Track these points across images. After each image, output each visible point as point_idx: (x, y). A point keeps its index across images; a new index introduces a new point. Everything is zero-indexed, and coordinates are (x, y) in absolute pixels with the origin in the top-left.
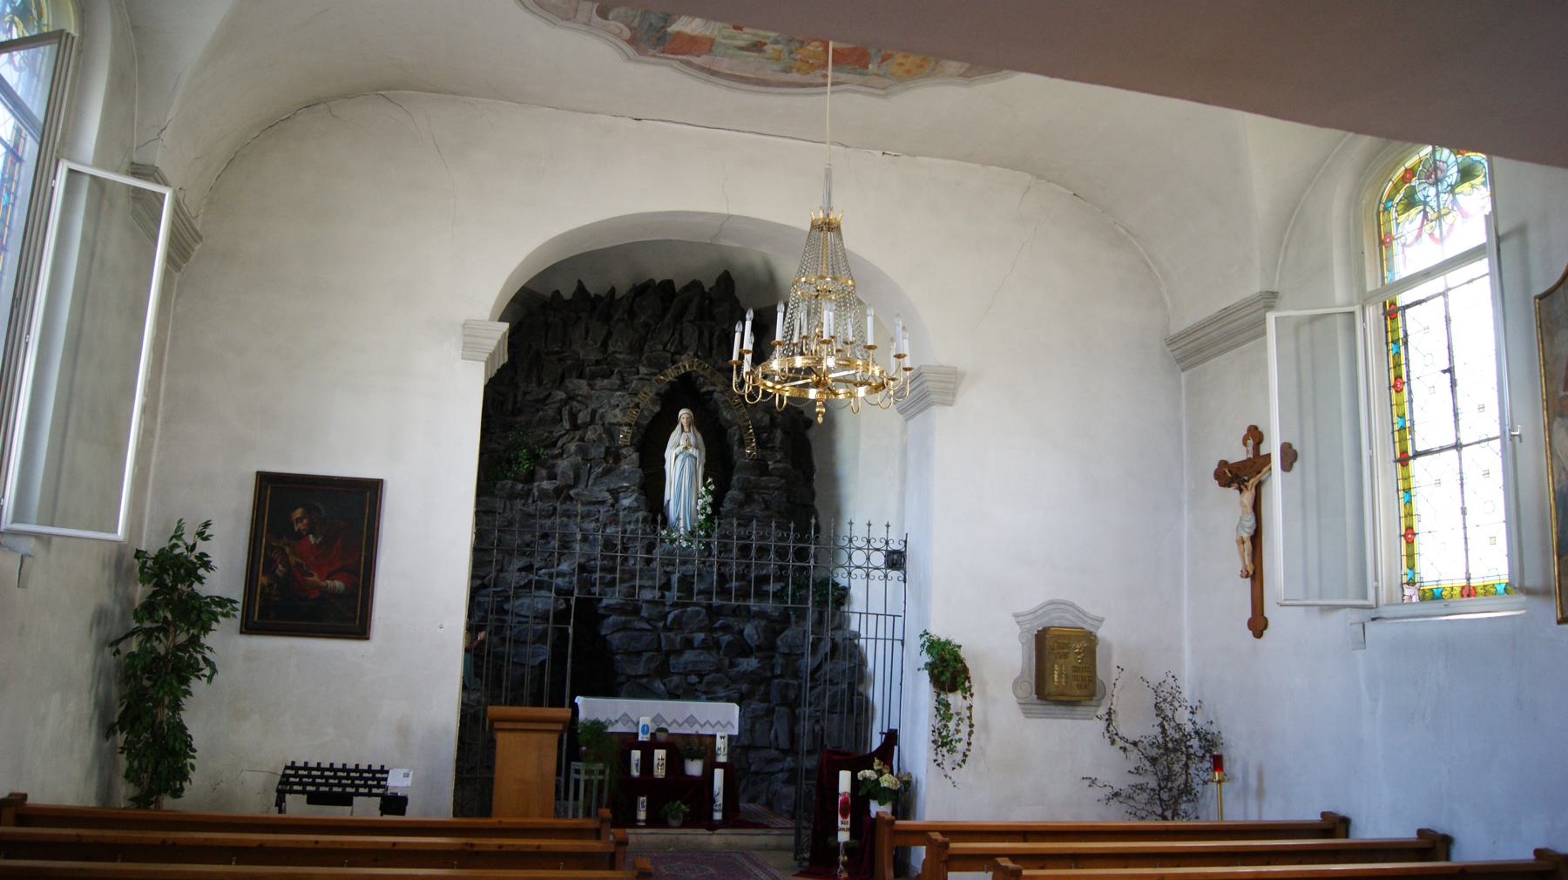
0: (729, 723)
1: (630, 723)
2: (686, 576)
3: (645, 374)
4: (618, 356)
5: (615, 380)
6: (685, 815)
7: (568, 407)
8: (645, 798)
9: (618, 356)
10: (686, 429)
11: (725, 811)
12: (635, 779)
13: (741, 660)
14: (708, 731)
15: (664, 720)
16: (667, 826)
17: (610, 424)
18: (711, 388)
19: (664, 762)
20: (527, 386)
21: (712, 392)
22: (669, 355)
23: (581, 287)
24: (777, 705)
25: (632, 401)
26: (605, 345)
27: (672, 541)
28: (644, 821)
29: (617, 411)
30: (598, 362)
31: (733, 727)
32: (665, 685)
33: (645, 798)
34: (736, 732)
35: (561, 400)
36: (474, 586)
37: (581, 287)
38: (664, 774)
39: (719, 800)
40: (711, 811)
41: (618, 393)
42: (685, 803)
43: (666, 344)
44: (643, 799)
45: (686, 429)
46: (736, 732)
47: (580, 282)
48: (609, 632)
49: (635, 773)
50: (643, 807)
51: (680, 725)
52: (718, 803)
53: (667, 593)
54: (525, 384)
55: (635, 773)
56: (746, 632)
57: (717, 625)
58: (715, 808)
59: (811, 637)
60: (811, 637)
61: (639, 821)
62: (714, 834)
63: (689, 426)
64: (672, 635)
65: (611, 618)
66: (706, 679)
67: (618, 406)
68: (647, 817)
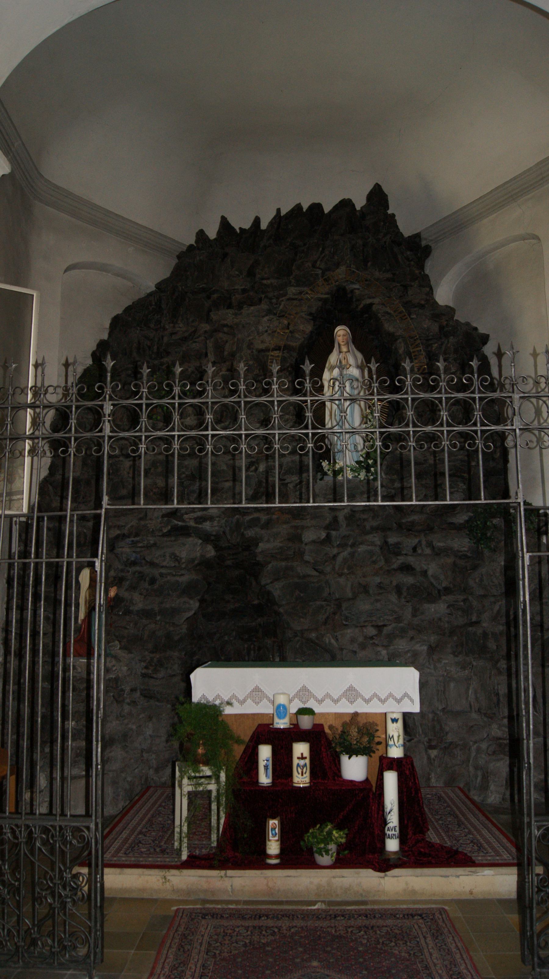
0: (406, 695)
1: (265, 700)
2: (354, 511)
3: (294, 295)
4: (265, 282)
5: (264, 306)
6: (341, 848)
7: (212, 340)
8: (276, 822)
9: (265, 282)
10: (344, 349)
11: (403, 839)
12: (265, 790)
13: (426, 606)
14: (375, 708)
15: (311, 695)
16: (313, 865)
17: (260, 351)
18: (368, 301)
19: (307, 761)
20: (174, 327)
21: (371, 304)
22: (320, 272)
23: (225, 224)
24: (268, 882)
25: (280, 323)
26: (251, 274)
27: (336, 473)
28: (277, 857)
29: (265, 337)
30: (244, 291)
31: (412, 701)
32: (337, 640)
33: (276, 822)
34: (416, 708)
35: (206, 332)
36: (111, 536)
37: (225, 224)
38: (307, 780)
39: (393, 820)
40: (382, 838)
41: (265, 319)
42: (339, 827)
43: (316, 262)
44: (273, 823)
45: (344, 349)
46: (416, 708)
47: (224, 219)
48: (269, 581)
49: (265, 779)
50: (274, 836)
51: (336, 701)
52: (391, 825)
53: (334, 533)
54: (172, 325)
55: (265, 779)
56: (430, 573)
57: (395, 566)
58: (388, 833)
59: (527, 556)
60: (527, 556)
61: (270, 857)
62: (386, 875)
63: (347, 344)
64: (342, 580)
65: (270, 566)
66: (386, 630)
67: (266, 331)
68: (282, 849)
